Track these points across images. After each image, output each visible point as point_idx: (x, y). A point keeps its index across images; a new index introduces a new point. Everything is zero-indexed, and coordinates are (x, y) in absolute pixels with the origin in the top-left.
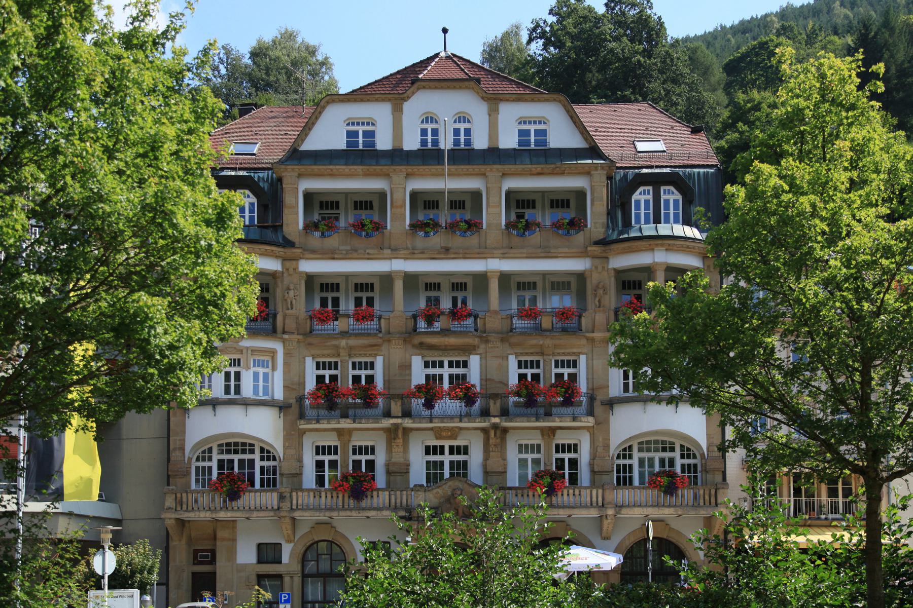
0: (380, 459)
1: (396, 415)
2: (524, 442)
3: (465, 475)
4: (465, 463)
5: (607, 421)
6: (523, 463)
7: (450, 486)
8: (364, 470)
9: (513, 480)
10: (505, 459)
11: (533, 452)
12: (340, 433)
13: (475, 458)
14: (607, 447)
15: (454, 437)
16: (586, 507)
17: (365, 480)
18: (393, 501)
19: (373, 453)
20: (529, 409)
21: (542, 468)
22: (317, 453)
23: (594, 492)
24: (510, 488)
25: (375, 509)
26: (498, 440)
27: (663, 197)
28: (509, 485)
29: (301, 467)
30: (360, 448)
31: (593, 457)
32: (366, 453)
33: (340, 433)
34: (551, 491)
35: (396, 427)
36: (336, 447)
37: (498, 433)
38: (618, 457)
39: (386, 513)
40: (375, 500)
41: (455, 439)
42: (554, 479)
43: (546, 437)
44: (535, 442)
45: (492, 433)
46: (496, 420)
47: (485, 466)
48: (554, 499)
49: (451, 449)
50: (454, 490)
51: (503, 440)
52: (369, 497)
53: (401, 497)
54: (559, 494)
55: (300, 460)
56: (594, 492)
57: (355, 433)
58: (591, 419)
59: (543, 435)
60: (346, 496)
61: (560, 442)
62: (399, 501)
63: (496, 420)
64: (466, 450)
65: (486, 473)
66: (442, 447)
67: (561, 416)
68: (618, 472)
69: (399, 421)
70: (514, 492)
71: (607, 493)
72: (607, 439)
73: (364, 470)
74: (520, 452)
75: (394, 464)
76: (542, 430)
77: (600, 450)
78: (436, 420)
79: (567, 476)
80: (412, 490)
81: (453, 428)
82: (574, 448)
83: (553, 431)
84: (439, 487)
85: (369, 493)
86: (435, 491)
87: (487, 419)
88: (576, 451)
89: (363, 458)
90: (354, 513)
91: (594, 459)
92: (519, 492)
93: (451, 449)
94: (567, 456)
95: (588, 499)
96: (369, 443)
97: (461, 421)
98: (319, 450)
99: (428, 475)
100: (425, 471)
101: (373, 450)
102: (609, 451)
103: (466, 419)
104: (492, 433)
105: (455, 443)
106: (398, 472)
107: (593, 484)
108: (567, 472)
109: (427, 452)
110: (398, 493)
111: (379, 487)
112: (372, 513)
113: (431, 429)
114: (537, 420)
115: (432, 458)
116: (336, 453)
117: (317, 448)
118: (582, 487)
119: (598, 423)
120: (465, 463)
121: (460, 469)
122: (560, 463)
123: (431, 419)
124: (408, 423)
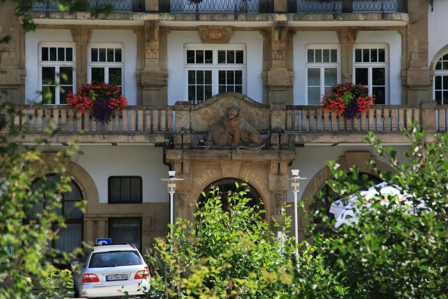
0: (129, 67)
1: (152, 9)
2: (315, 47)
3: (239, 89)
4: (239, 74)
5: (424, 20)
6: (313, 75)
7: (222, 104)
8: (107, 81)
9: (301, 97)
10: (291, 70)
11: (326, 60)
12: (76, 31)
13: (253, 69)
14: (424, 53)
15: (225, 40)
16: (398, 132)
17: (112, 96)
18: (148, 123)
19: (119, 59)
20: (324, 4)
21: (339, 82)
22: (45, 58)
23: (409, 113)
24: (300, 108)
25: (124, 133)
26: (284, 45)
27: (139, 113)
28: (296, 103)
29: (23, 75)
30: (102, 51)
31: (406, 66)
32: (110, 60)
33: (76, 31)
34: (352, 111)
35: (152, 23)
36: (69, 50)
37: (284, 34)
38: (438, 67)
39: (140, 139)
40: (125, 121)
41: (227, 42)
42: (353, 98)
43: (344, 41)
44: (330, 47)
45: (276, 35)
46: (282, 18)
47: (265, 78)
48: (356, 122)
49: (221, 54)
50: (229, 109)
51: (289, 44)
52: (117, 117)
53: (159, 118)
54: (364, 114)
55: (22, 67)
56: (409, 113)
57: (95, 32)
58: (405, 16)
59: (340, 38)
60: (87, 115)
61: (362, 47)
62: (156, 123)
63: (282, 18)
64: (239, 57)
65: (267, 87)
66: (209, 54)
67: (366, 13)
68: (438, 86)
69: (156, 17)
70: (305, 112)
71: (426, 114)
72: (424, 43)
73: (107, 81)
74: (310, 60)
75: (148, 74)
76: (339, 31)
77: (415, 57)
78: (204, 17)
79: (370, 93)
80: (173, 108)
81: (224, 27)
82: (380, 55)
83: (353, 32)
84: (208, 105)
85: (117, 112)
86: (203, 110)
87: (270, 16)
88: (382, 59)
89: (107, 66)
90: (97, 139)
91: (407, 69)
92: (312, 112)
93: (221, 54)
94: (370, 66)
95: (402, 122)
96: (114, 47)
97: (236, 18)
98: (46, 54)
99: (191, 89)
100: (186, 85)
101: (118, 56)
102: (427, 60)
103: (242, 16)
104: (276, 35)
105: (226, 48)
106: (152, 85)
107: (406, 102)
108: (370, 86)
109: (190, 60)
110: (155, 112)
111: (129, 104)
112: (122, 139)
113: (196, 29)
114: (335, 18)
115: (196, 67)
116: (70, 58)
117: (45, 50)
118: (391, 107)
119: (412, 22)
120: (239, 74)
121: (231, 82)
122: (362, 74)
123: (197, 16)
124: (167, 20)
